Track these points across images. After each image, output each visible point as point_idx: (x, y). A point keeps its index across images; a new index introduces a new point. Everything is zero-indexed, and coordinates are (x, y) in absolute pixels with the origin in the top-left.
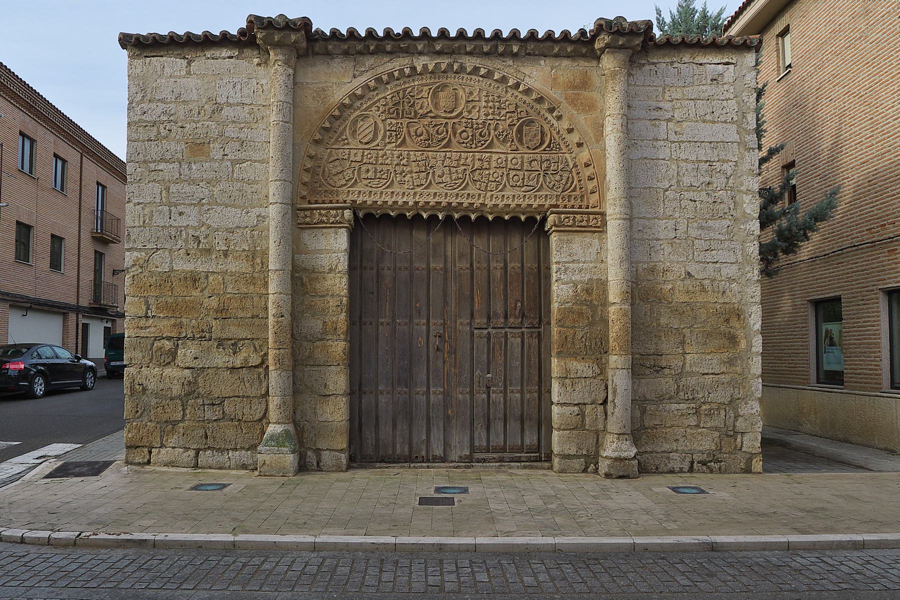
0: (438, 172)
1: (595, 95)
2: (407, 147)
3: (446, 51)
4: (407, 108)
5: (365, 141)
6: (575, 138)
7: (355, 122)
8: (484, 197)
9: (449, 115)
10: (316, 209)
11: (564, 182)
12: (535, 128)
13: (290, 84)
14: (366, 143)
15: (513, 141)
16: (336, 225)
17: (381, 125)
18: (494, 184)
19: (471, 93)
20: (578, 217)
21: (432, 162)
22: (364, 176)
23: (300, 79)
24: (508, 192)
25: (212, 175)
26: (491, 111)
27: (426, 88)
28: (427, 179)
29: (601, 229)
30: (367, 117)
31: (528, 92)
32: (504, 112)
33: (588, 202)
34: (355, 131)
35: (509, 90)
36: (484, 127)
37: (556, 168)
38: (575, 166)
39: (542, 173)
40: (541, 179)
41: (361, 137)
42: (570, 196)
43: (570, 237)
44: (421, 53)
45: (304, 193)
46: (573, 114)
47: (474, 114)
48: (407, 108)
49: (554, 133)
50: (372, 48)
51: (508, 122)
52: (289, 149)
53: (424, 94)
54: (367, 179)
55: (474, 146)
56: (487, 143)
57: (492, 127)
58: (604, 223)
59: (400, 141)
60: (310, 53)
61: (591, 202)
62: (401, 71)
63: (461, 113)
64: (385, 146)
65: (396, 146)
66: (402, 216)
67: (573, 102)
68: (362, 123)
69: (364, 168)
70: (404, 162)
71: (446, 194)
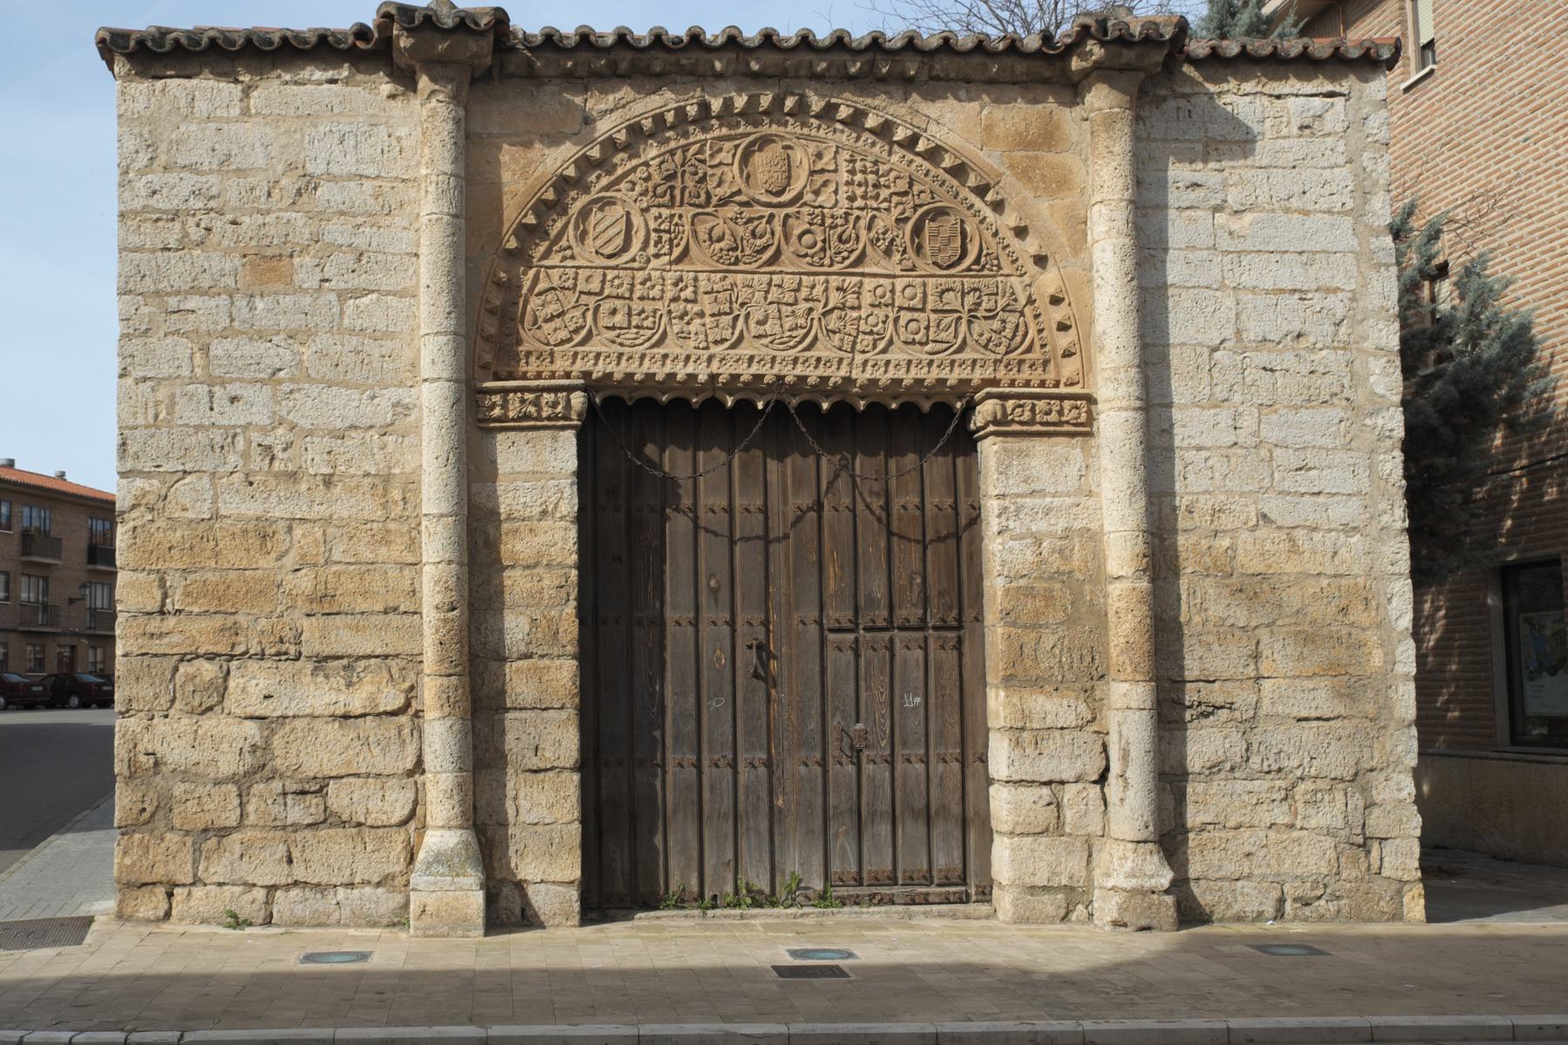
2: (692, 263)
4: (690, 184)
5: (608, 250)
7: (585, 213)
8: (851, 364)
9: (776, 200)
11: (1008, 333)
12: (948, 224)
14: (610, 257)
15: (904, 252)
16: (554, 424)
17: (637, 220)
19: (819, 156)
20: (1041, 405)
22: (604, 321)
25: (297, 322)
26: (859, 191)
27: (728, 145)
28: (734, 327)
29: (1084, 431)
30: (611, 202)
32: (884, 193)
33: (1058, 373)
34: (584, 234)
35: (896, 148)
36: (847, 221)
37: (991, 305)
38: (1031, 301)
39: (965, 316)
40: (963, 327)
41: (599, 242)
42: (1021, 362)
43: (1025, 443)
44: (719, 76)
45: (488, 358)
46: (1025, 198)
48: (690, 184)
50: (624, 66)
51: (895, 212)
53: (724, 157)
54: (613, 328)
55: (827, 261)
57: (863, 223)
58: (1091, 419)
59: (677, 252)
62: (680, 112)
63: (800, 196)
64: (648, 261)
65: (670, 263)
69: (606, 306)
70: (688, 293)
71: (773, 359)
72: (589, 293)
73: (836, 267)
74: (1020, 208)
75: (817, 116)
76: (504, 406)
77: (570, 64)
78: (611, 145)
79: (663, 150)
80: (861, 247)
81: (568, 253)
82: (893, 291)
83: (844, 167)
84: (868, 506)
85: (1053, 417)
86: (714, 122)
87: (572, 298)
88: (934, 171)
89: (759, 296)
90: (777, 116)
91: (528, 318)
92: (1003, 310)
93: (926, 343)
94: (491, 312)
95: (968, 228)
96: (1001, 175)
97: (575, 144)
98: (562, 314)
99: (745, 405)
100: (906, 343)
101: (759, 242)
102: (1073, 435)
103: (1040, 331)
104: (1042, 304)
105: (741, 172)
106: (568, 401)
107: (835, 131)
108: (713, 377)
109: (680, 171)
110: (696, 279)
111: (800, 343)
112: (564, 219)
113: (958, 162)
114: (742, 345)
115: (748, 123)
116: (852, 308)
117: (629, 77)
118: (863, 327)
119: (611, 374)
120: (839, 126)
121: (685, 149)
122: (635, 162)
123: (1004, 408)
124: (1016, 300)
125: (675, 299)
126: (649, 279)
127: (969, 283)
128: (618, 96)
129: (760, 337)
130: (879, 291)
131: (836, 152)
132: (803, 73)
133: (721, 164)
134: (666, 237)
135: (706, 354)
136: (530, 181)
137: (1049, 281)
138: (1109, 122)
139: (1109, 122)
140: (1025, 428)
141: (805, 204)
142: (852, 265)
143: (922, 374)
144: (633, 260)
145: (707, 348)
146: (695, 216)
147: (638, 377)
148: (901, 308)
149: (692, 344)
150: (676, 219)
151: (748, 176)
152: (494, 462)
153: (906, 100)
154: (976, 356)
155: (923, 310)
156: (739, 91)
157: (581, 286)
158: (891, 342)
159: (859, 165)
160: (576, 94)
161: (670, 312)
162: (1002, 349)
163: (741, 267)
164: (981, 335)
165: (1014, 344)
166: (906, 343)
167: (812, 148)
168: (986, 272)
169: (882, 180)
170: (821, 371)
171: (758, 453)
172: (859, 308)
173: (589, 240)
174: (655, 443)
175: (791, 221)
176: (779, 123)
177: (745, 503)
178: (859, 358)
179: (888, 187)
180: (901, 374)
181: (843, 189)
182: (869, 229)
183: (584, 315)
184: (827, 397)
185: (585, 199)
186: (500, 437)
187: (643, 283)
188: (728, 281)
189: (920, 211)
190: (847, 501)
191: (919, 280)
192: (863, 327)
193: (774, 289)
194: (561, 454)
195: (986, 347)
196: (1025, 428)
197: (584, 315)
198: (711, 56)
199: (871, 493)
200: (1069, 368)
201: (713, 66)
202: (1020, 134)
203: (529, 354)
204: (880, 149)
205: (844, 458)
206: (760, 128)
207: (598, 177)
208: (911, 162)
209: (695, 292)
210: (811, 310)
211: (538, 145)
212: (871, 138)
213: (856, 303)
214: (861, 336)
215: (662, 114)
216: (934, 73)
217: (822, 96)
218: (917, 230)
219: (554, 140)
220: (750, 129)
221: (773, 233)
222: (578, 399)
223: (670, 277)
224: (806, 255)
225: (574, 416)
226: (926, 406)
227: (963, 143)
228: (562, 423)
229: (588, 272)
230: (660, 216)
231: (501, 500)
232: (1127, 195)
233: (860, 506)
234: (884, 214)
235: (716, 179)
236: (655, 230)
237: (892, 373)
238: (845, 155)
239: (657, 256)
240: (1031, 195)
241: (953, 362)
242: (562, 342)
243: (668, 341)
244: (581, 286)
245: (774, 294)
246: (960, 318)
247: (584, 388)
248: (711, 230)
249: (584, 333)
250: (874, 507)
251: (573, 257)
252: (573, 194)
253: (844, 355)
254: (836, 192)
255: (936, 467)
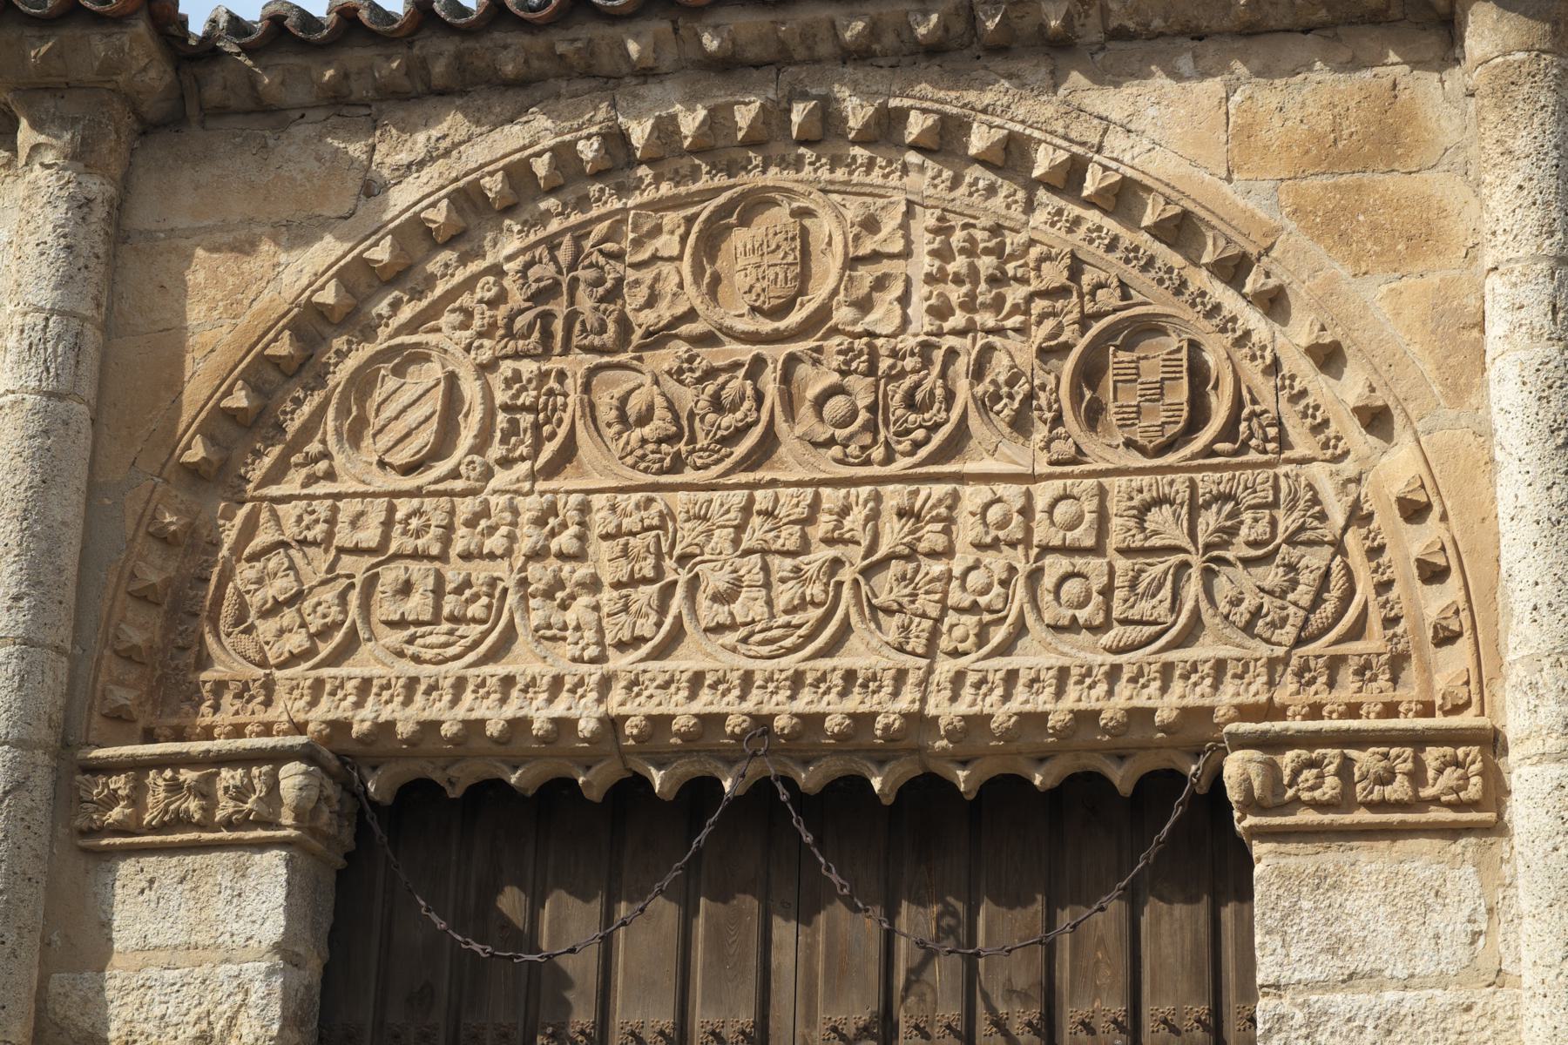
0: (715, 579)
1: (1441, 185)
2: (583, 474)
3: (752, 53)
4: (585, 302)
5: (402, 456)
6: (1345, 392)
7: (363, 382)
8: (924, 683)
9: (767, 326)
10: (160, 763)
11: (1303, 594)
12: (1156, 357)
13: (94, 240)
14: (408, 470)
15: (1058, 420)
16: (244, 833)
17: (470, 389)
18: (970, 621)
19: (870, 224)
20: (1366, 760)
21: (688, 535)
22: (386, 608)
23: (143, 216)
24: (1035, 656)
26: (956, 294)
27: (671, 218)
28: (662, 610)
29: (1480, 819)
30: (419, 356)
31: (1122, 198)
32: (1015, 294)
33: (1429, 682)
34: (361, 424)
35: (1042, 194)
36: (927, 362)
37: (1262, 528)
38: (1358, 516)
39: (1197, 560)
40: (1193, 588)
41: (385, 441)
42: (1335, 663)
43: (1332, 857)
44: (646, 74)
45: (123, 696)
46: (1333, 279)
47: (883, 316)
48: (585, 302)
49: (1253, 373)
50: (439, 68)
51: (1039, 334)
52: (68, 508)
53: (667, 244)
54: (401, 624)
55: (878, 453)
56: (938, 438)
57: (962, 365)
58: (1496, 791)
59: (549, 449)
60: (192, 110)
61: (1440, 683)
62: (564, 155)
63: (824, 312)
64: (488, 474)
65: (533, 476)
66: (559, 791)
67: (1332, 226)
68: (392, 383)
69: (391, 576)
70: (565, 541)
71: (747, 678)
72: (357, 551)
73: (900, 465)
74: (1320, 304)
75: (860, 141)
76: (137, 798)
77: (329, 73)
78: (418, 237)
79: (532, 238)
80: (955, 415)
81: (322, 466)
82: (1027, 511)
83: (924, 243)
84: (999, 1024)
85: (1398, 789)
86: (643, 171)
87: (322, 559)
88: (1127, 237)
89: (722, 537)
90: (777, 149)
91: (228, 610)
92: (1291, 541)
93: (1105, 627)
94: (144, 597)
95: (1210, 358)
96: (1278, 231)
97: (340, 238)
98: (297, 598)
99: (701, 791)
100: (1056, 628)
101: (727, 420)
102: (1453, 832)
103: (1384, 587)
104: (1387, 520)
105: (698, 271)
106: (273, 785)
107: (905, 169)
108: (612, 724)
109: (565, 280)
110: (585, 508)
111: (810, 638)
112: (318, 397)
113: (1173, 210)
114: (681, 650)
115: (715, 168)
116: (933, 554)
117: (463, 93)
118: (956, 596)
119: (390, 725)
120: (913, 158)
121: (579, 233)
122: (474, 267)
123: (1272, 769)
124: (1323, 517)
125: (537, 555)
126: (485, 512)
127: (1207, 483)
128: (435, 133)
129: (719, 629)
130: (994, 514)
131: (909, 213)
132: (824, 49)
133: (655, 258)
134: (526, 420)
135: (594, 673)
136: (243, 321)
137: (1396, 468)
138: (1503, 88)
139: (1503, 88)
140: (1327, 818)
141: (835, 331)
142: (932, 459)
143: (1093, 699)
144: (455, 474)
145: (600, 659)
146: (593, 371)
147: (447, 730)
148: (1046, 550)
149: (570, 650)
150: (552, 383)
151: (716, 280)
152: (106, 925)
153: (1055, 88)
154: (1224, 651)
155: (1097, 550)
156: (690, 102)
157: (344, 537)
158: (1021, 629)
159: (958, 238)
160: (352, 137)
161: (523, 583)
162: (1287, 634)
163: (689, 476)
164: (1236, 602)
165: (1316, 620)
166: (1056, 628)
167: (854, 209)
168: (1253, 456)
169: (1010, 268)
170: (853, 703)
171: (749, 904)
172: (948, 553)
173: (367, 442)
174: (522, 888)
175: (803, 370)
176: (784, 163)
177: (714, 1020)
178: (945, 667)
179: (1024, 281)
180: (1043, 701)
181: (920, 291)
182: (978, 373)
183: (343, 597)
184: (881, 763)
185: (366, 351)
186: (126, 868)
187: (471, 523)
188: (656, 508)
189: (1097, 327)
190: (951, 1011)
191: (1090, 483)
192: (956, 596)
193: (756, 521)
194: (252, 905)
195: (1248, 628)
196: (1327, 818)
197: (343, 597)
198: (618, 30)
199: (1010, 992)
200: (1450, 668)
201: (626, 54)
202: (1320, 139)
203: (220, 687)
204: (1004, 201)
205: (948, 911)
206: (742, 177)
207: (395, 306)
208: (1077, 221)
209: (582, 538)
210: (837, 563)
211: (266, 247)
212: (986, 177)
213: (940, 542)
214: (952, 617)
215: (525, 164)
216: (1114, 23)
217: (870, 95)
218: (1090, 372)
219: (299, 234)
220: (721, 180)
221: (759, 398)
222: (291, 777)
223: (530, 506)
224: (831, 442)
225: (287, 818)
226: (1122, 777)
227: (1185, 169)
228: (260, 833)
229: (356, 505)
230: (517, 376)
231: (112, 1010)
232: (1549, 246)
233: (983, 1026)
234: (1014, 342)
235: (643, 293)
236: (506, 408)
237: (1021, 701)
238: (929, 219)
239: (506, 462)
240: (1345, 272)
241: (1167, 670)
242: (293, 659)
243: (518, 648)
244: (344, 537)
245: (756, 533)
246: (1186, 565)
247: (306, 755)
248: (624, 400)
249: (338, 637)
250: (1016, 1027)
251: (330, 475)
252: (339, 343)
253: (909, 661)
254: (904, 300)
255: (1171, 927)
